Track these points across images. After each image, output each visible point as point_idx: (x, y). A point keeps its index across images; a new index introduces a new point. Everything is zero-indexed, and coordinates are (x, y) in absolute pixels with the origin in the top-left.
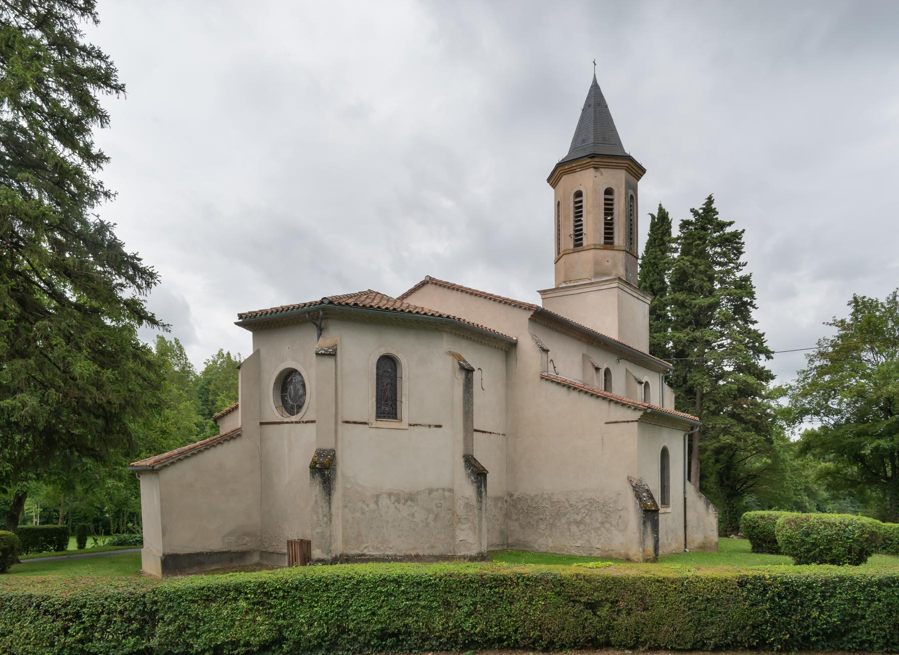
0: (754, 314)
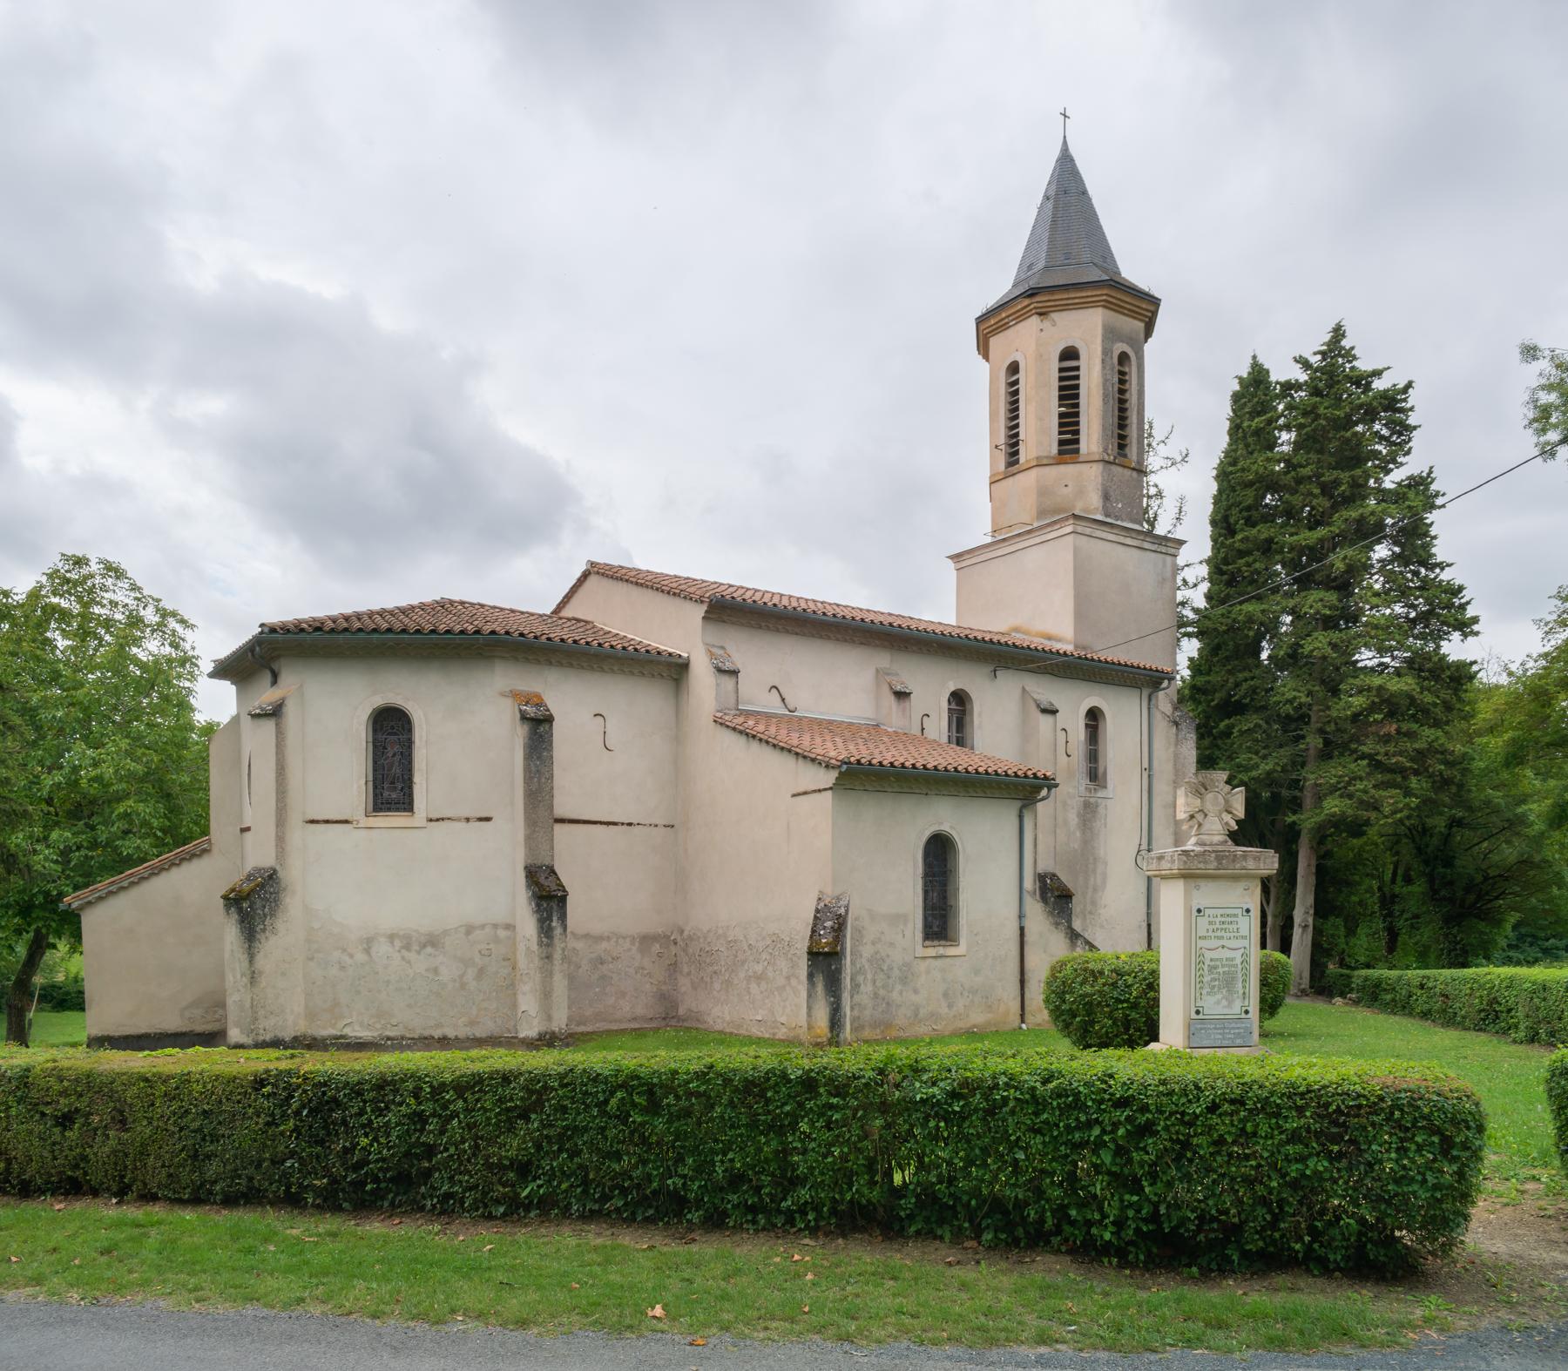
0: (1440, 552)
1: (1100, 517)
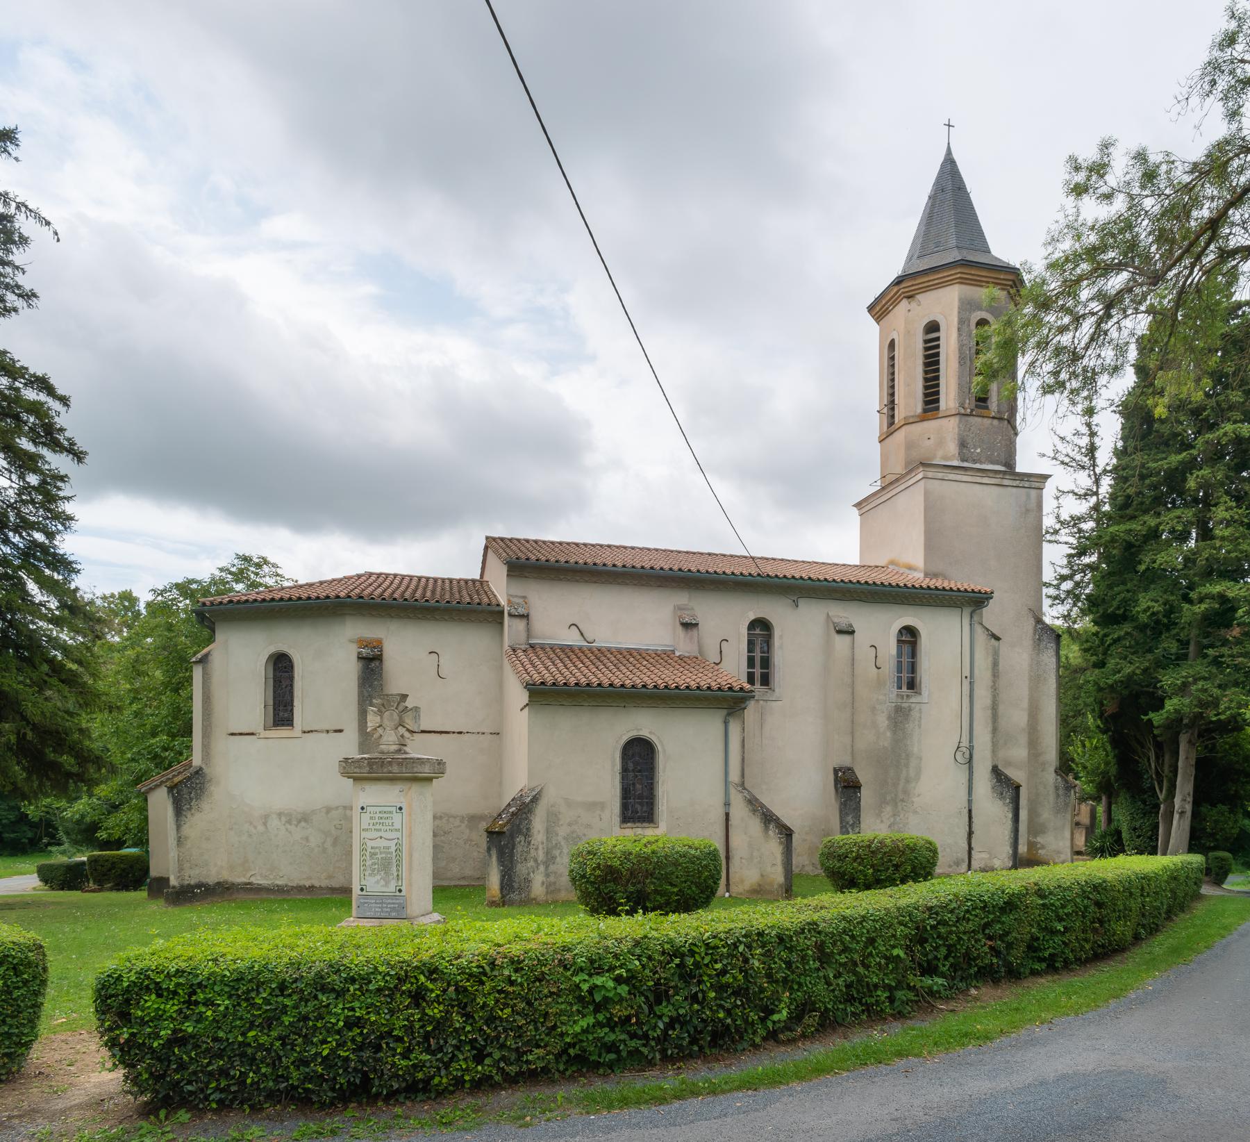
1: (956, 463)
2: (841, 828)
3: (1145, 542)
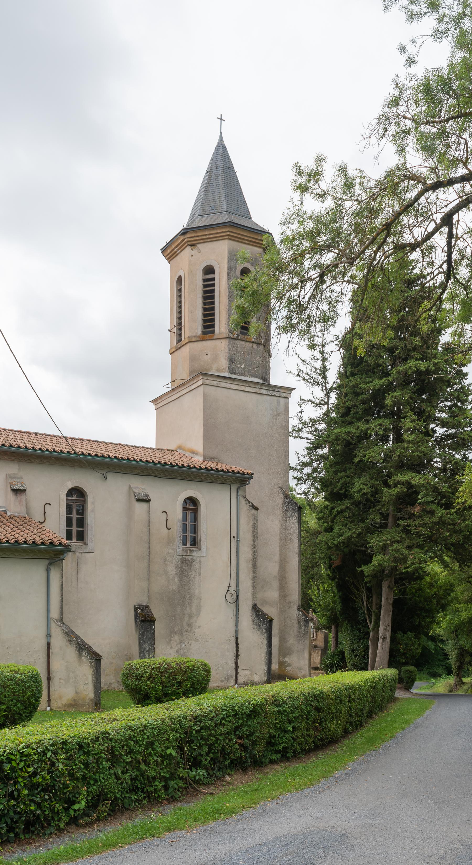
1: (226, 374)
2: (140, 653)
3: (359, 441)
